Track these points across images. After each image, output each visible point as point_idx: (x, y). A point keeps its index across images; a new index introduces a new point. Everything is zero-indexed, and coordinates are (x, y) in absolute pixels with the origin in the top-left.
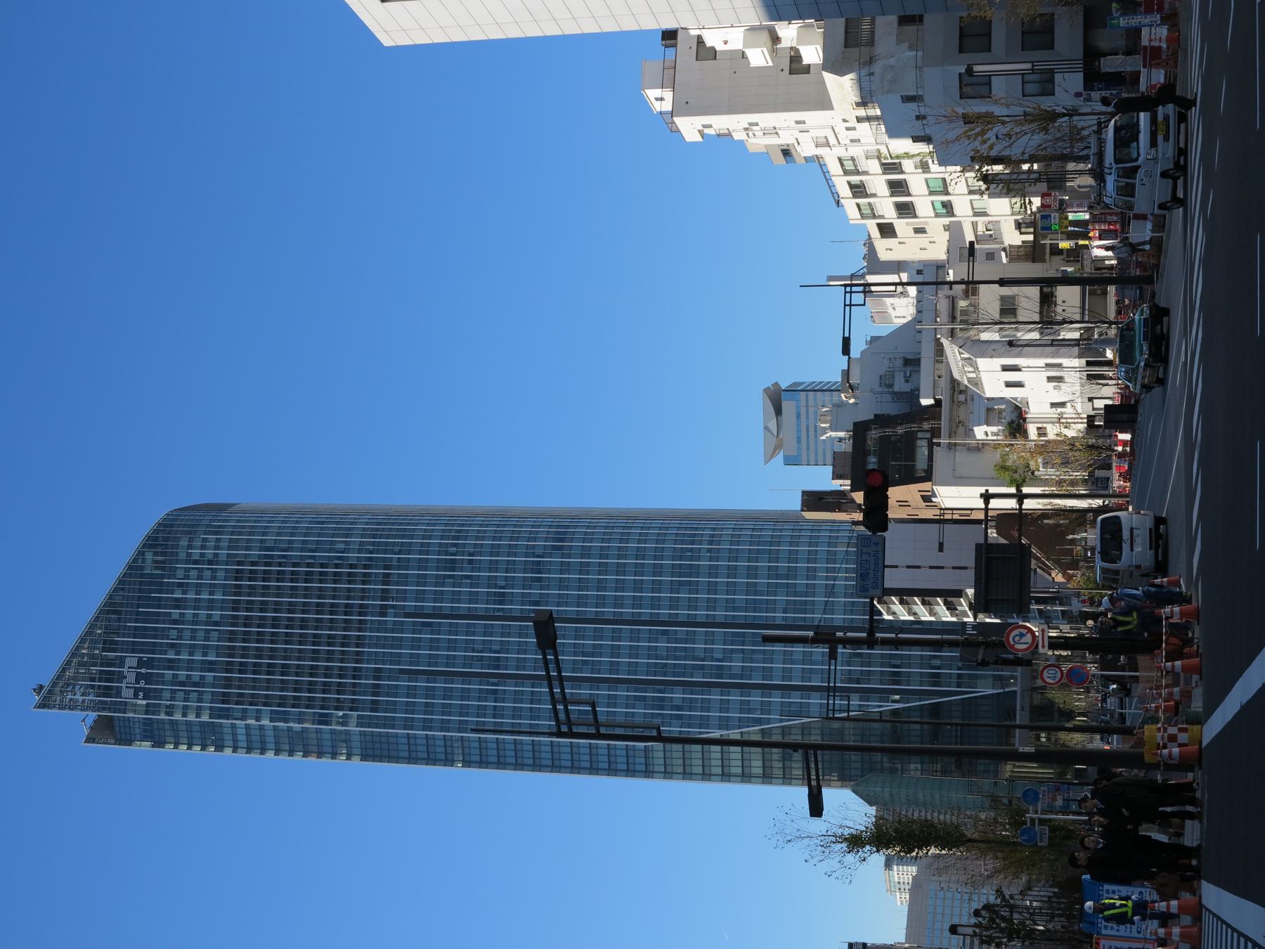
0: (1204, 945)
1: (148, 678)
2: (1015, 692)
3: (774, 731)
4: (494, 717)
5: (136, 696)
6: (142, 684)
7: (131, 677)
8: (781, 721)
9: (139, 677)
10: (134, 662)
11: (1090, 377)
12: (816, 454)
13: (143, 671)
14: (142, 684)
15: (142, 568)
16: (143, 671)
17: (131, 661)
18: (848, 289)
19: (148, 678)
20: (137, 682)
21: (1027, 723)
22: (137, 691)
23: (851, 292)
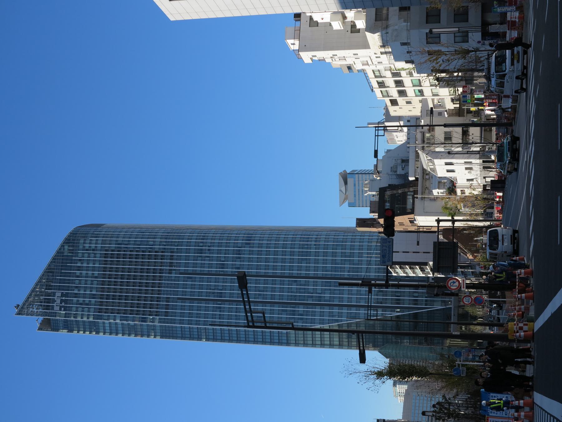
0: (535, 420)
1: (66, 302)
2: (451, 308)
3: (344, 325)
5: (60, 310)
6: (63, 304)
7: (58, 301)
8: (347, 321)
9: (62, 301)
10: (60, 294)
11: (484, 168)
12: (363, 202)
13: (64, 298)
14: (63, 304)
15: (63, 253)
16: (64, 298)
17: (58, 294)
18: (377, 129)
19: (66, 302)
20: (61, 303)
21: (456, 322)
22: (61, 307)
23: (378, 130)
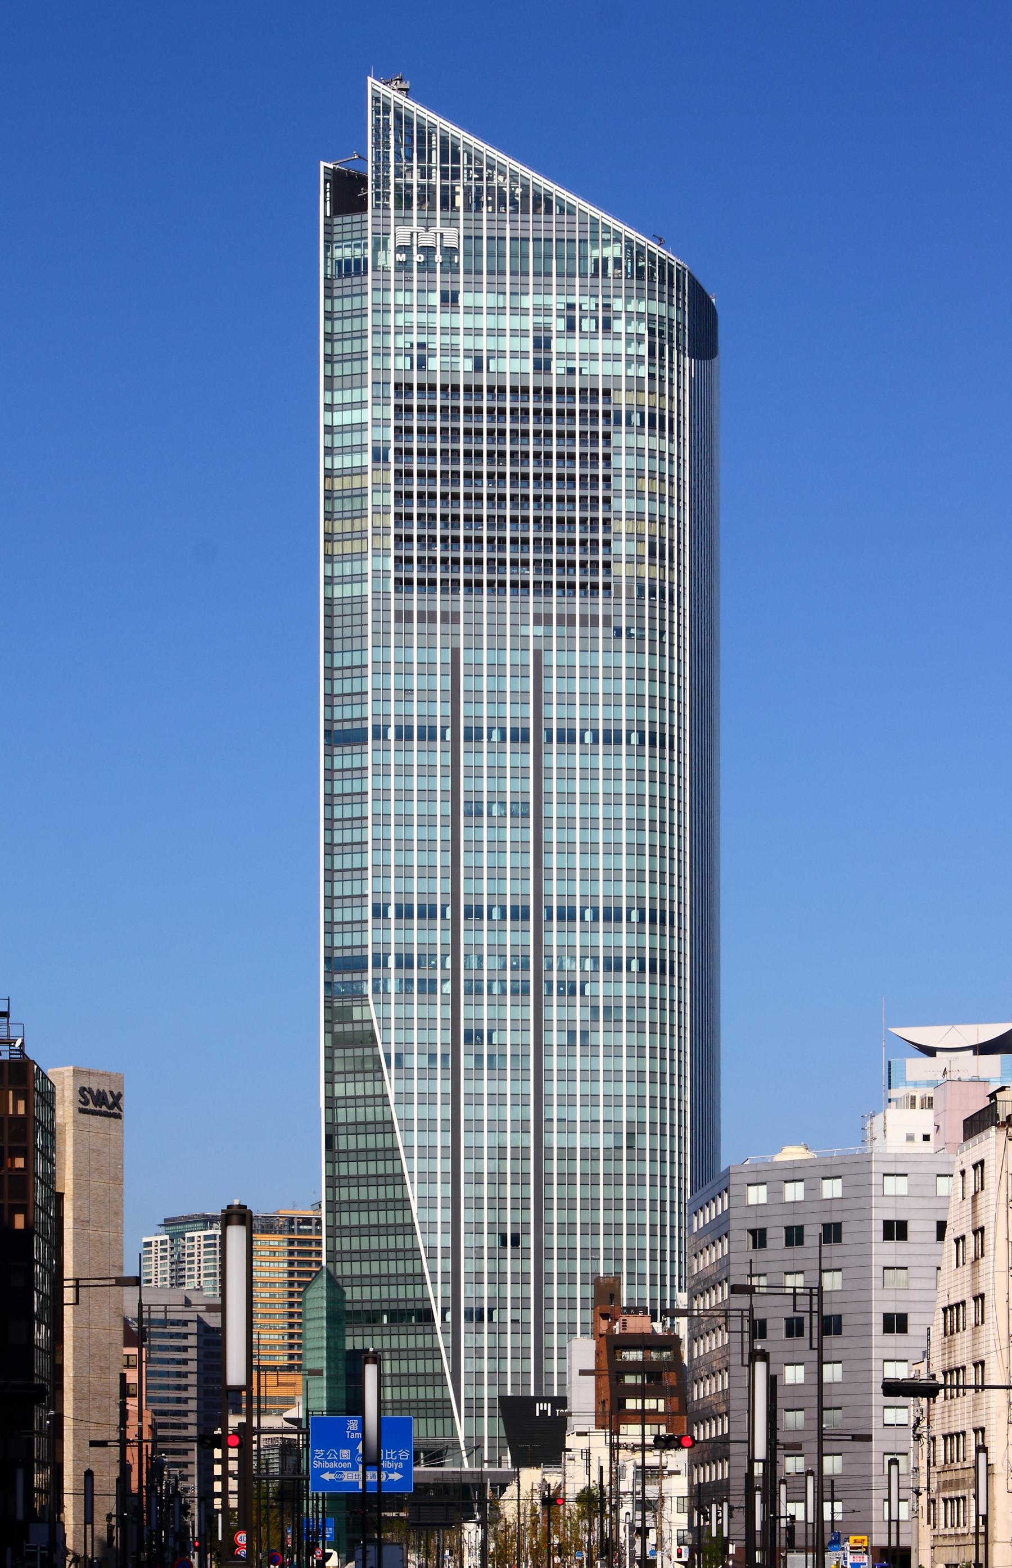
0: (999, 1555)
1: (427, 267)
2: (462, 1465)
3: (437, 1362)
4: (481, 273)
7: (427, 240)
8: (411, 1173)
9: (428, 251)
13: (438, 258)
14: (417, 258)
15: (595, 241)
16: (438, 258)
17: (453, 237)
18: (815, 1291)
19: (427, 267)
20: (422, 249)
23: (811, 1295)
